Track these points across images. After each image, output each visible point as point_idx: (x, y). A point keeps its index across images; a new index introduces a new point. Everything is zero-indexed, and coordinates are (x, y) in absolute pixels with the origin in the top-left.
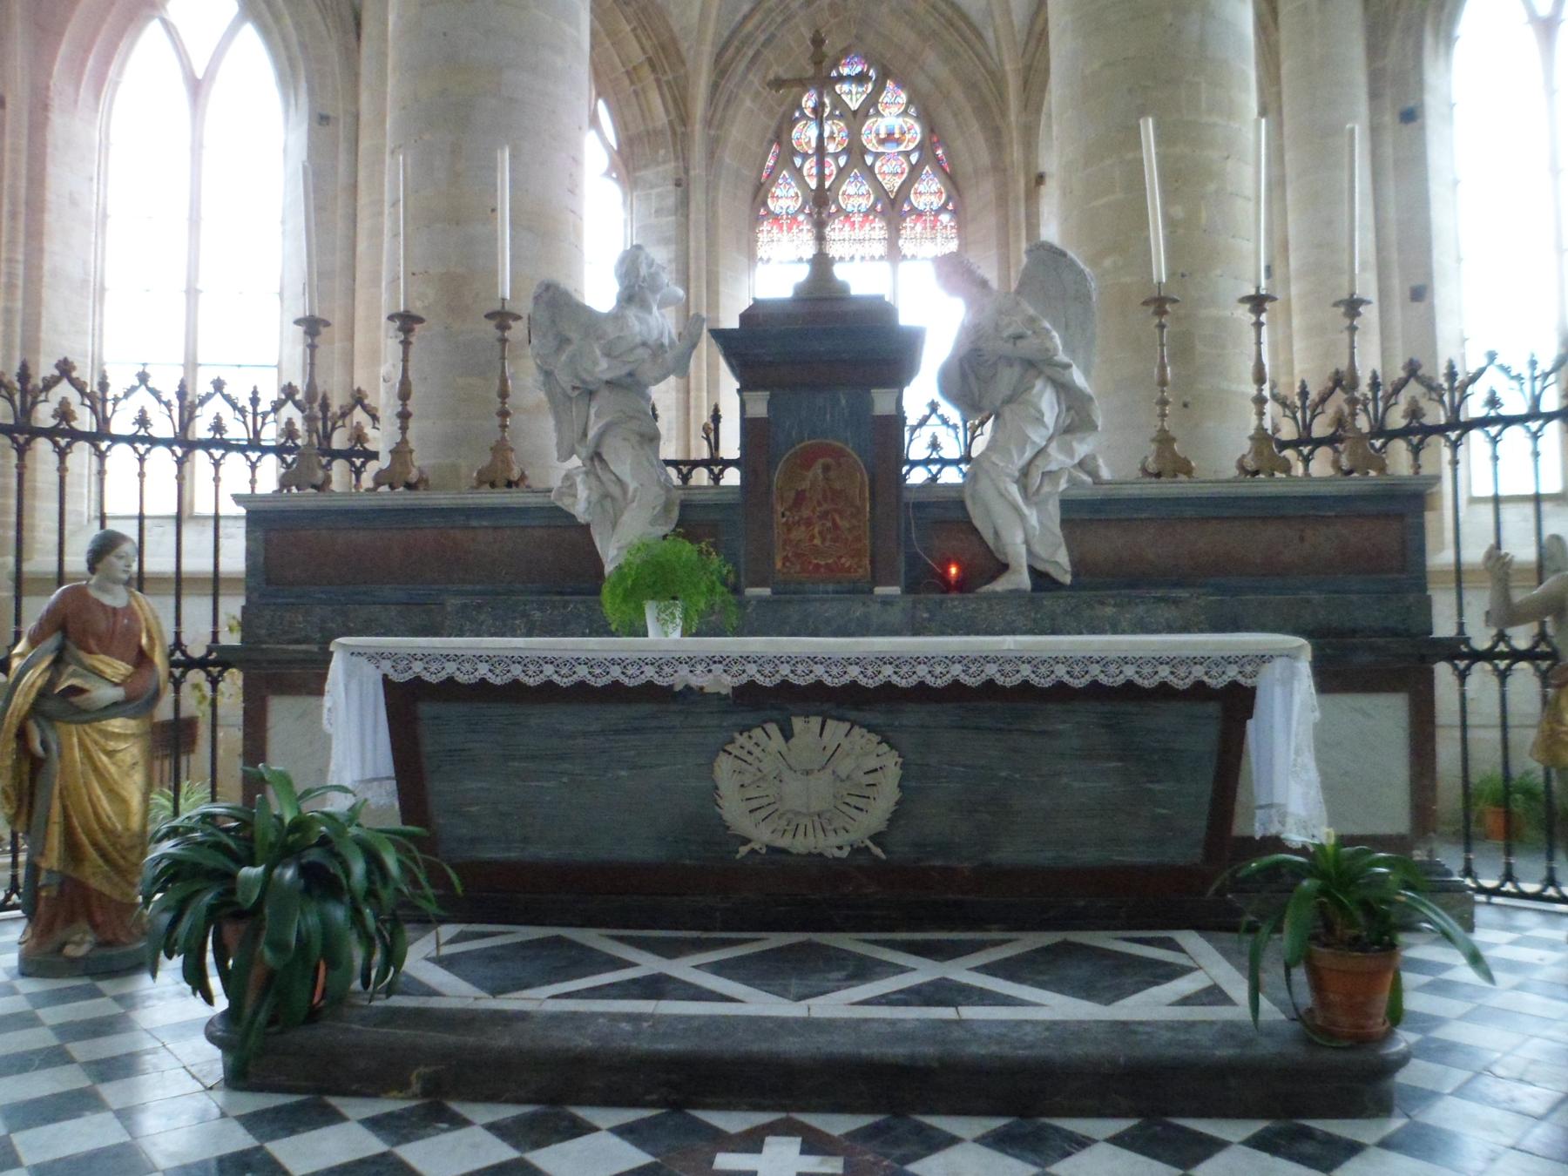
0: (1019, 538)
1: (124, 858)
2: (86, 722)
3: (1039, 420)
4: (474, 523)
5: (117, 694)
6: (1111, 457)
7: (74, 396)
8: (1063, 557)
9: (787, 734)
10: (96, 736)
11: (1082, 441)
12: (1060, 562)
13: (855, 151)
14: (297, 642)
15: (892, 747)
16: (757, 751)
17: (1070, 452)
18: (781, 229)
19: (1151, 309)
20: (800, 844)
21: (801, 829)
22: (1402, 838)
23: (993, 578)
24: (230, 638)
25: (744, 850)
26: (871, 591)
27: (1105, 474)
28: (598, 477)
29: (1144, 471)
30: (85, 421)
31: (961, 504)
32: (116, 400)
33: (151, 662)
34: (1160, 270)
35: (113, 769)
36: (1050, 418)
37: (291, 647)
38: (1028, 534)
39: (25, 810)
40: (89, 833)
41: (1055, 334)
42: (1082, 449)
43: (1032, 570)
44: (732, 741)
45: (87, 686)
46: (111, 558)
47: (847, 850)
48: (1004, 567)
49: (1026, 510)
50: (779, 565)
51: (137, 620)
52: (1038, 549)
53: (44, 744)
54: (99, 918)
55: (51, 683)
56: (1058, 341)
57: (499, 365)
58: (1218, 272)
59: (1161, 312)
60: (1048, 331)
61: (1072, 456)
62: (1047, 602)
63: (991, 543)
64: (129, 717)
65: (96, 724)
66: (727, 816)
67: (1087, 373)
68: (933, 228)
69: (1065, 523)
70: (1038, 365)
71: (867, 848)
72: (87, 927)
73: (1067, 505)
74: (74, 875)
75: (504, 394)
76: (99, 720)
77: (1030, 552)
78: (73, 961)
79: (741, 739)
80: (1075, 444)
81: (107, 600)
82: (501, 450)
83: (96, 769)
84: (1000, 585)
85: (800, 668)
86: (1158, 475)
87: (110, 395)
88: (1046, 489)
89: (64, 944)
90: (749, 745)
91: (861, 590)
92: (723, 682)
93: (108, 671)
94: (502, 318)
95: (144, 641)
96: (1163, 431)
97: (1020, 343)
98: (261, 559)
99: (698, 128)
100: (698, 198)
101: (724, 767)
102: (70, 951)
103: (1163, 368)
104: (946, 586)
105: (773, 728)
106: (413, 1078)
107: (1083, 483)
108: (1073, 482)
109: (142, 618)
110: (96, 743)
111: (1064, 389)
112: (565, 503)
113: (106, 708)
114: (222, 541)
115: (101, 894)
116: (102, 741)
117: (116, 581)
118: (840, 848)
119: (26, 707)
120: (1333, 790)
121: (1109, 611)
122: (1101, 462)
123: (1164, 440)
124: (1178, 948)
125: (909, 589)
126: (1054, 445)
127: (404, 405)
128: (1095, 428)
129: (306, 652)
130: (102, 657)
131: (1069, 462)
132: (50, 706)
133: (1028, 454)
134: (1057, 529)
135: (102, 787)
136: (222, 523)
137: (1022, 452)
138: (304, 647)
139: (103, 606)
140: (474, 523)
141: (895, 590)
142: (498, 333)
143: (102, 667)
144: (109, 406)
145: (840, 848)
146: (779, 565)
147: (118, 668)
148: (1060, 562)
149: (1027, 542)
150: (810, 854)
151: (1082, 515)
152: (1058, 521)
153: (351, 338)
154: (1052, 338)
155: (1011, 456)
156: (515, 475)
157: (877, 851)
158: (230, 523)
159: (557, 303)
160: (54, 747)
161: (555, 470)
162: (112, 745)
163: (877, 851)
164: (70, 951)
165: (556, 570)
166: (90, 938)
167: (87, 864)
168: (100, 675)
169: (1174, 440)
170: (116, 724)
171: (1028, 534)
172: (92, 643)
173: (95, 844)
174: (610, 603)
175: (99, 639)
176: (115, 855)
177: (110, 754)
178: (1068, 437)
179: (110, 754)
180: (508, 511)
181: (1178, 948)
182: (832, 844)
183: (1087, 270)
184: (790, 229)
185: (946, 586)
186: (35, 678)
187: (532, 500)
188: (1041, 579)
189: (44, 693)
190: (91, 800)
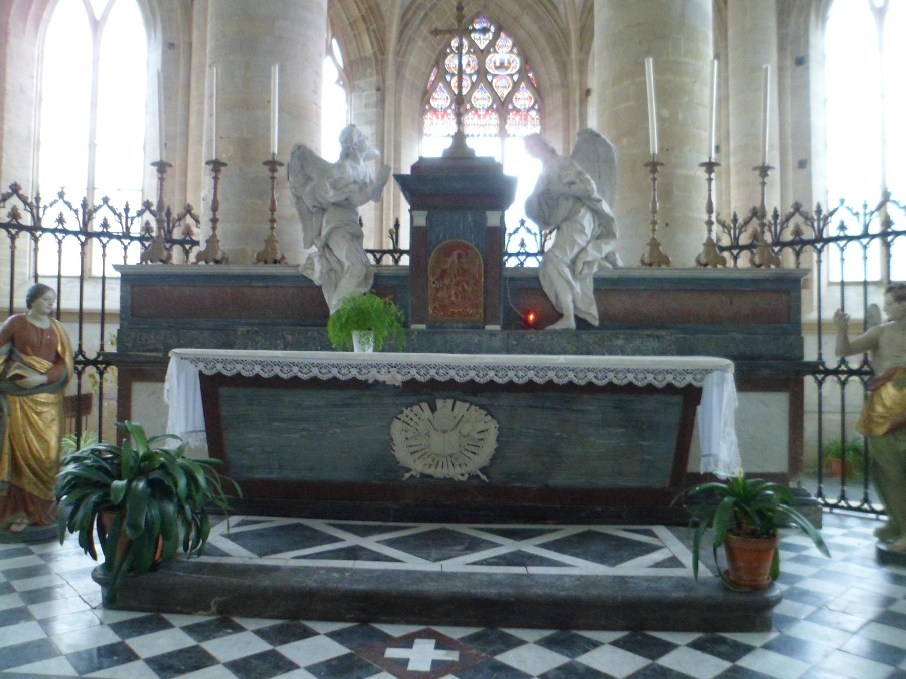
1: (46, 475)
2: (26, 395)
3: (582, 231)
5: (43, 379)
6: (624, 254)
7: (20, 205)
9: (433, 409)
10: (31, 404)
11: (607, 244)
12: (593, 313)
13: (482, 72)
14: (150, 351)
20: (439, 472)
21: (440, 464)
24: (111, 348)
25: (407, 475)
26: (483, 328)
27: (620, 263)
28: (327, 259)
30: (26, 219)
31: (536, 279)
32: (45, 207)
35: (40, 423)
37: (148, 354)
38: (575, 297)
41: (593, 182)
42: (607, 248)
43: (576, 317)
44: (401, 413)
46: (40, 300)
47: (466, 476)
48: (560, 316)
49: (574, 283)
50: (431, 312)
54: (31, 509)
58: (688, 148)
62: (585, 336)
65: (31, 397)
67: (611, 205)
68: (526, 119)
69: (597, 291)
70: (583, 200)
71: (478, 476)
75: (273, 209)
76: (33, 394)
78: (16, 533)
79: (406, 412)
80: (603, 246)
81: (38, 324)
82: (271, 242)
84: (558, 326)
86: (651, 265)
87: (41, 205)
88: (585, 271)
90: (411, 415)
91: (478, 327)
92: (396, 378)
93: (38, 366)
94: (273, 165)
95: (60, 348)
96: (654, 239)
97: (573, 187)
99: (390, 58)
100: (389, 98)
102: (14, 528)
104: (527, 325)
105: (425, 406)
106: (212, 603)
107: (607, 268)
108: (601, 267)
110: (30, 408)
111: (597, 213)
112: (307, 273)
113: (37, 387)
115: (32, 496)
117: (43, 314)
118: (462, 475)
120: (746, 446)
122: (617, 256)
123: (654, 244)
127: (214, 215)
128: (615, 237)
130: (34, 357)
131: (599, 256)
133: (576, 251)
137: (572, 250)
138: (154, 354)
141: (497, 328)
142: (270, 173)
144: (41, 211)
145: (462, 475)
146: (431, 312)
147: (44, 364)
148: (593, 313)
149: (574, 301)
150: (445, 478)
151: (605, 287)
153: (185, 175)
155: (565, 251)
156: (279, 256)
157: (483, 477)
161: (302, 254)
162: (40, 409)
163: (483, 477)
164: (14, 528)
165: (301, 312)
170: (42, 397)
171: (575, 297)
172: (29, 350)
173: (29, 466)
174: (332, 332)
175: (32, 346)
176: (41, 473)
177: (39, 414)
178: (599, 242)
182: (457, 473)
185: (527, 325)
187: (288, 271)
188: (581, 323)
190: (27, 441)
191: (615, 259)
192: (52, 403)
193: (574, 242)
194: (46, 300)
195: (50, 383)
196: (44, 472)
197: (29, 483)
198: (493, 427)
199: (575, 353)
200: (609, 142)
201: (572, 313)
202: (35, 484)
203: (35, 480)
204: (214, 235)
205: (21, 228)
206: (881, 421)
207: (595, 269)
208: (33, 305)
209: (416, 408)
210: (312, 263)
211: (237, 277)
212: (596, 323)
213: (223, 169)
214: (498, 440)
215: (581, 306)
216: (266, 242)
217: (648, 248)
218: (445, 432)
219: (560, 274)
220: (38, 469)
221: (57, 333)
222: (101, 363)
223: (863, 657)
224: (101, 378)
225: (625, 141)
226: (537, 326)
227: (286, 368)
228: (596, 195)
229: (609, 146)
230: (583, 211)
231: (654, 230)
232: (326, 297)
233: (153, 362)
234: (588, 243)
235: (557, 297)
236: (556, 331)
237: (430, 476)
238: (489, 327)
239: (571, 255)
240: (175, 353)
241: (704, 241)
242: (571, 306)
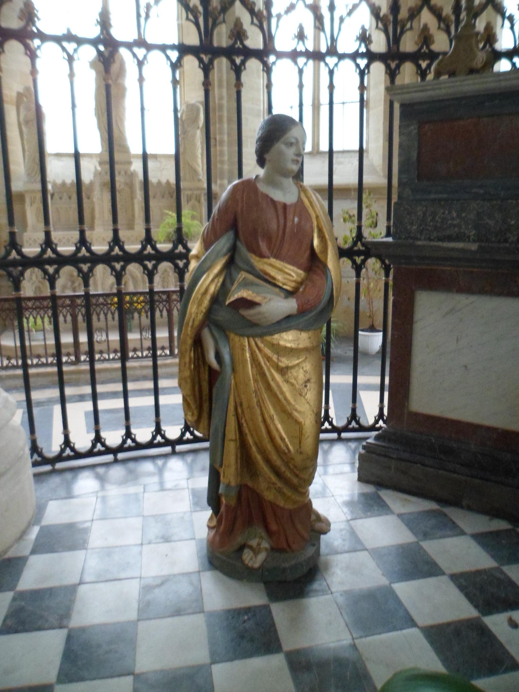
1: (297, 476)
2: (261, 336)
5: (290, 305)
7: (246, 18)
10: (268, 351)
14: (450, 238)
24: (377, 233)
30: (254, 40)
32: (279, 16)
35: (285, 388)
37: (446, 245)
39: (205, 415)
40: (262, 451)
45: (257, 299)
46: (280, 146)
51: (308, 218)
53: (218, 356)
54: (274, 527)
55: (224, 290)
64: (301, 330)
65: (268, 338)
72: (264, 534)
74: (250, 484)
76: (272, 334)
81: (278, 196)
83: (269, 387)
87: (274, 11)
89: (241, 548)
93: (280, 277)
95: (316, 242)
98: (414, 154)
109: (313, 216)
110: (269, 359)
113: (279, 322)
114: (335, 166)
115: (274, 506)
116: (275, 358)
117: (285, 174)
119: (200, 317)
129: (463, 250)
130: (272, 260)
132: (223, 315)
135: (274, 407)
136: (335, 156)
138: (460, 245)
139: (273, 202)
143: (273, 272)
144: (274, 21)
147: (288, 274)
158: (340, 155)
160: (227, 358)
162: (284, 362)
164: (247, 556)
166: (265, 545)
167: (261, 479)
168: (271, 282)
170: (288, 339)
172: (263, 246)
173: (268, 461)
175: (269, 239)
176: (288, 474)
177: (283, 371)
179: (283, 371)
186: (209, 283)
189: (217, 300)
190: (264, 421)
192: (306, 350)
194: (291, 144)
195: (302, 312)
196: (291, 471)
197: (269, 488)
202: (279, 491)
203: (279, 484)
205: (248, 53)
208: (267, 157)
220: (283, 469)
221: (311, 210)
222: (359, 253)
224: (358, 275)
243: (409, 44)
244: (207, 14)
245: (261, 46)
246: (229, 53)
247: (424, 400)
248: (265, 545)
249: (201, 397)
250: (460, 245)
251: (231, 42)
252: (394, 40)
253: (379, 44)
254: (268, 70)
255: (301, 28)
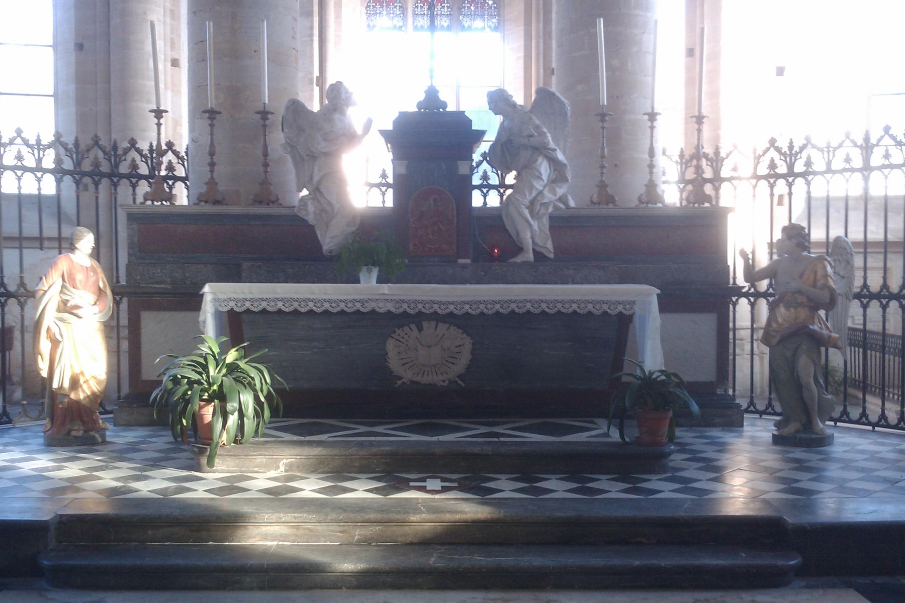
0: (529, 235)
3: (539, 178)
4: (252, 223)
8: (550, 245)
9: (420, 329)
11: (560, 187)
12: (548, 246)
14: (158, 283)
15: (468, 335)
16: (406, 337)
17: (555, 194)
18: (382, 7)
19: (599, 118)
20: (426, 379)
21: (426, 373)
22: (711, 383)
23: (514, 256)
25: (399, 382)
26: (456, 262)
27: (572, 204)
28: (318, 200)
29: (592, 202)
31: (500, 217)
33: (106, 293)
34: (604, 100)
36: (545, 177)
41: (549, 135)
42: (560, 191)
43: (534, 250)
44: (395, 332)
47: (447, 382)
48: (520, 250)
49: (532, 222)
50: (411, 248)
52: (538, 241)
56: (550, 139)
57: (262, 139)
58: (636, 95)
59: (603, 121)
60: (545, 133)
61: (555, 194)
62: (543, 269)
63: (514, 237)
66: (391, 366)
67: (564, 153)
68: (482, 8)
69: (551, 228)
70: (542, 150)
71: (456, 382)
73: (552, 218)
75: (266, 154)
77: (533, 242)
78: (76, 437)
79: (399, 331)
80: (557, 189)
82: (265, 183)
84: (519, 259)
85: (536, 305)
86: (599, 204)
88: (542, 211)
89: (70, 431)
90: (402, 334)
94: (264, 114)
96: (602, 181)
97: (531, 139)
101: (390, 345)
102: (74, 433)
103: (603, 149)
105: (413, 326)
106: (281, 464)
107: (561, 208)
108: (555, 207)
111: (553, 161)
112: (302, 214)
118: (444, 381)
121: (571, 272)
122: (570, 198)
123: (602, 186)
124: (595, 423)
125: (475, 260)
126: (547, 189)
127: (212, 159)
128: (567, 181)
131: (555, 198)
133: (534, 194)
134: (548, 233)
137: (531, 193)
138: (163, 286)
140: (252, 223)
141: (468, 261)
142: (262, 122)
145: (444, 381)
146: (411, 248)
148: (548, 246)
149: (532, 238)
150: (430, 384)
151: (561, 223)
152: (547, 226)
153: (109, 82)
154: (546, 137)
155: (525, 195)
156: (273, 199)
157: (460, 382)
159: (296, 108)
163: (460, 382)
164: (74, 433)
169: (607, 186)
171: (534, 234)
178: (554, 185)
180: (270, 217)
181: (595, 423)
182: (440, 379)
183: (566, 101)
184: (387, 6)
185: (492, 258)
187: (283, 211)
191: (567, 200)
193: (532, 187)
198: (468, 342)
199: (534, 283)
200: (563, 99)
201: (531, 247)
204: (212, 178)
206: (774, 334)
207: (551, 209)
209: (406, 329)
210: (305, 205)
211: (237, 217)
212: (552, 256)
213: (218, 116)
214: (472, 353)
215: (539, 241)
216: (261, 184)
217: (596, 190)
218: (429, 347)
219: (521, 215)
223: (344, 134)
225: (579, 88)
226: (502, 258)
227: (628, 306)
228: (552, 145)
229: (562, 102)
230: (540, 159)
231: (602, 173)
232: (319, 236)
233: (161, 293)
234: (545, 187)
235: (518, 234)
236: (516, 263)
237: (417, 383)
238: (461, 261)
239: (529, 197)
240: (207, 289)
241: (646, 182)
242: (530, 241)
243: (87, 166)
244: (77, 153)
245: (184, 175)
246: (128, 176)
247: (793, 221)
248: (82, 428)
249: (118, 352)
250: (163, 286)
251: (481, 182)
252: (78, 164)
253: (68, 165)
254: (808, 183)
255: (384, 171)
